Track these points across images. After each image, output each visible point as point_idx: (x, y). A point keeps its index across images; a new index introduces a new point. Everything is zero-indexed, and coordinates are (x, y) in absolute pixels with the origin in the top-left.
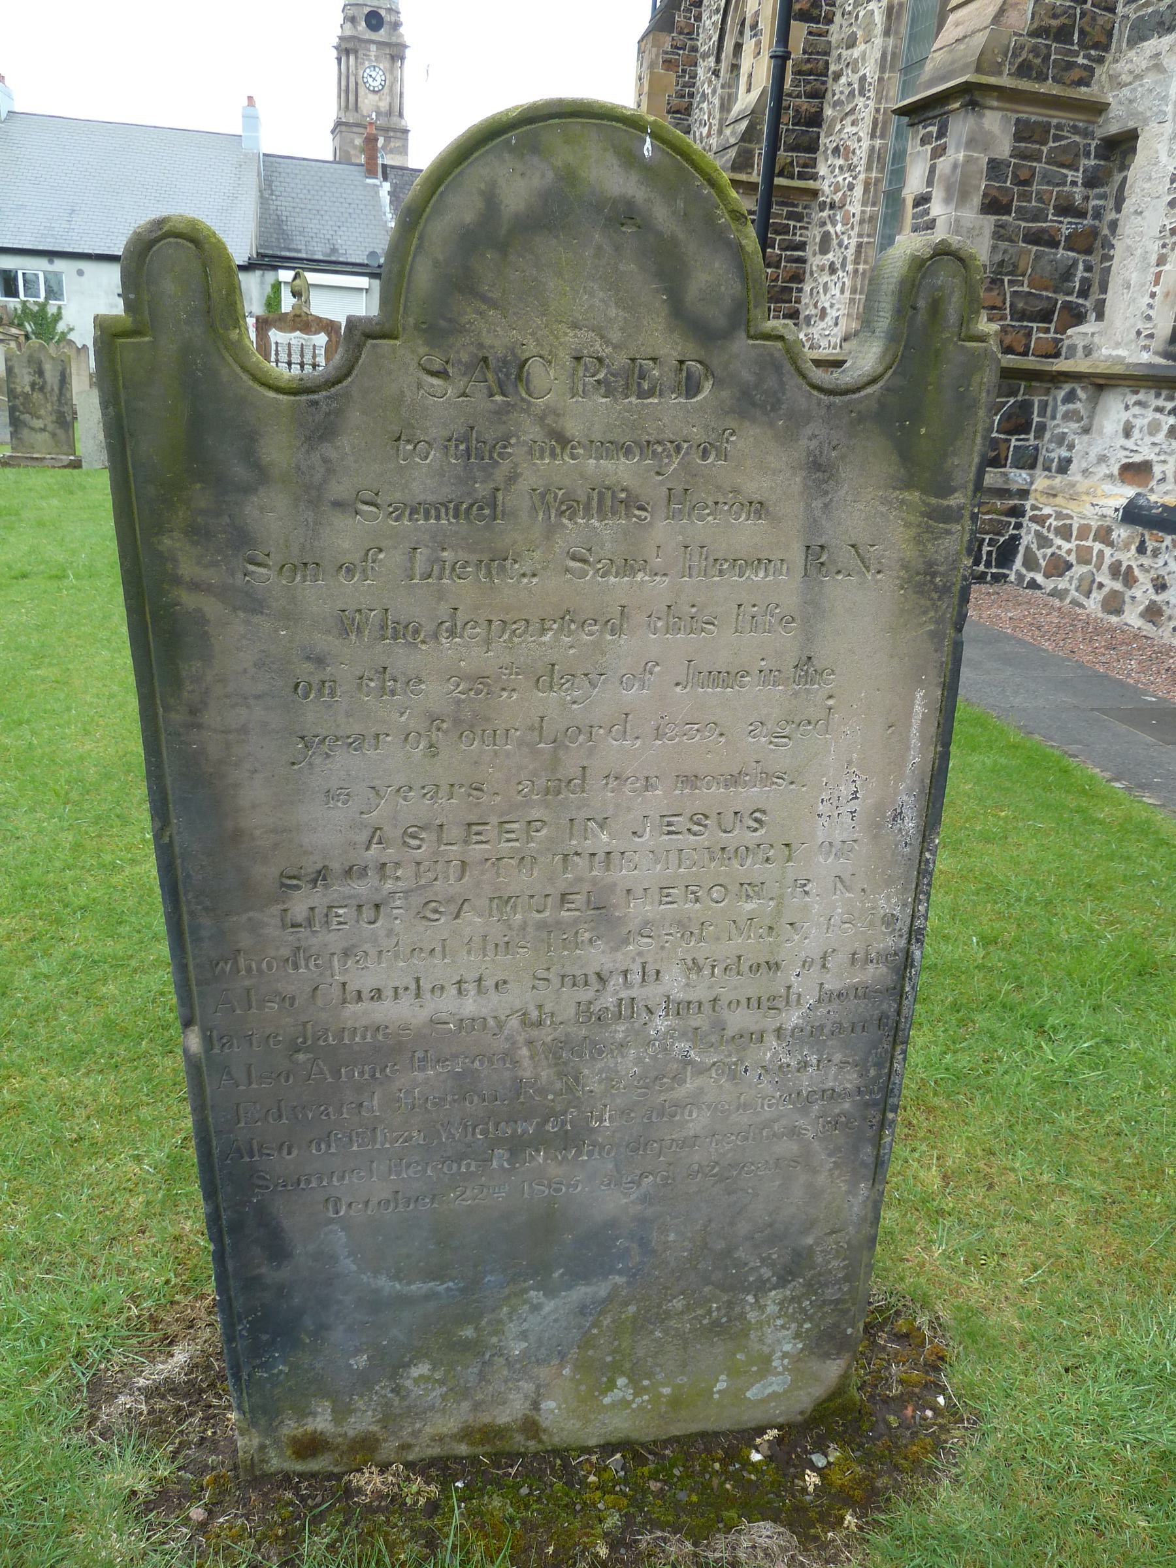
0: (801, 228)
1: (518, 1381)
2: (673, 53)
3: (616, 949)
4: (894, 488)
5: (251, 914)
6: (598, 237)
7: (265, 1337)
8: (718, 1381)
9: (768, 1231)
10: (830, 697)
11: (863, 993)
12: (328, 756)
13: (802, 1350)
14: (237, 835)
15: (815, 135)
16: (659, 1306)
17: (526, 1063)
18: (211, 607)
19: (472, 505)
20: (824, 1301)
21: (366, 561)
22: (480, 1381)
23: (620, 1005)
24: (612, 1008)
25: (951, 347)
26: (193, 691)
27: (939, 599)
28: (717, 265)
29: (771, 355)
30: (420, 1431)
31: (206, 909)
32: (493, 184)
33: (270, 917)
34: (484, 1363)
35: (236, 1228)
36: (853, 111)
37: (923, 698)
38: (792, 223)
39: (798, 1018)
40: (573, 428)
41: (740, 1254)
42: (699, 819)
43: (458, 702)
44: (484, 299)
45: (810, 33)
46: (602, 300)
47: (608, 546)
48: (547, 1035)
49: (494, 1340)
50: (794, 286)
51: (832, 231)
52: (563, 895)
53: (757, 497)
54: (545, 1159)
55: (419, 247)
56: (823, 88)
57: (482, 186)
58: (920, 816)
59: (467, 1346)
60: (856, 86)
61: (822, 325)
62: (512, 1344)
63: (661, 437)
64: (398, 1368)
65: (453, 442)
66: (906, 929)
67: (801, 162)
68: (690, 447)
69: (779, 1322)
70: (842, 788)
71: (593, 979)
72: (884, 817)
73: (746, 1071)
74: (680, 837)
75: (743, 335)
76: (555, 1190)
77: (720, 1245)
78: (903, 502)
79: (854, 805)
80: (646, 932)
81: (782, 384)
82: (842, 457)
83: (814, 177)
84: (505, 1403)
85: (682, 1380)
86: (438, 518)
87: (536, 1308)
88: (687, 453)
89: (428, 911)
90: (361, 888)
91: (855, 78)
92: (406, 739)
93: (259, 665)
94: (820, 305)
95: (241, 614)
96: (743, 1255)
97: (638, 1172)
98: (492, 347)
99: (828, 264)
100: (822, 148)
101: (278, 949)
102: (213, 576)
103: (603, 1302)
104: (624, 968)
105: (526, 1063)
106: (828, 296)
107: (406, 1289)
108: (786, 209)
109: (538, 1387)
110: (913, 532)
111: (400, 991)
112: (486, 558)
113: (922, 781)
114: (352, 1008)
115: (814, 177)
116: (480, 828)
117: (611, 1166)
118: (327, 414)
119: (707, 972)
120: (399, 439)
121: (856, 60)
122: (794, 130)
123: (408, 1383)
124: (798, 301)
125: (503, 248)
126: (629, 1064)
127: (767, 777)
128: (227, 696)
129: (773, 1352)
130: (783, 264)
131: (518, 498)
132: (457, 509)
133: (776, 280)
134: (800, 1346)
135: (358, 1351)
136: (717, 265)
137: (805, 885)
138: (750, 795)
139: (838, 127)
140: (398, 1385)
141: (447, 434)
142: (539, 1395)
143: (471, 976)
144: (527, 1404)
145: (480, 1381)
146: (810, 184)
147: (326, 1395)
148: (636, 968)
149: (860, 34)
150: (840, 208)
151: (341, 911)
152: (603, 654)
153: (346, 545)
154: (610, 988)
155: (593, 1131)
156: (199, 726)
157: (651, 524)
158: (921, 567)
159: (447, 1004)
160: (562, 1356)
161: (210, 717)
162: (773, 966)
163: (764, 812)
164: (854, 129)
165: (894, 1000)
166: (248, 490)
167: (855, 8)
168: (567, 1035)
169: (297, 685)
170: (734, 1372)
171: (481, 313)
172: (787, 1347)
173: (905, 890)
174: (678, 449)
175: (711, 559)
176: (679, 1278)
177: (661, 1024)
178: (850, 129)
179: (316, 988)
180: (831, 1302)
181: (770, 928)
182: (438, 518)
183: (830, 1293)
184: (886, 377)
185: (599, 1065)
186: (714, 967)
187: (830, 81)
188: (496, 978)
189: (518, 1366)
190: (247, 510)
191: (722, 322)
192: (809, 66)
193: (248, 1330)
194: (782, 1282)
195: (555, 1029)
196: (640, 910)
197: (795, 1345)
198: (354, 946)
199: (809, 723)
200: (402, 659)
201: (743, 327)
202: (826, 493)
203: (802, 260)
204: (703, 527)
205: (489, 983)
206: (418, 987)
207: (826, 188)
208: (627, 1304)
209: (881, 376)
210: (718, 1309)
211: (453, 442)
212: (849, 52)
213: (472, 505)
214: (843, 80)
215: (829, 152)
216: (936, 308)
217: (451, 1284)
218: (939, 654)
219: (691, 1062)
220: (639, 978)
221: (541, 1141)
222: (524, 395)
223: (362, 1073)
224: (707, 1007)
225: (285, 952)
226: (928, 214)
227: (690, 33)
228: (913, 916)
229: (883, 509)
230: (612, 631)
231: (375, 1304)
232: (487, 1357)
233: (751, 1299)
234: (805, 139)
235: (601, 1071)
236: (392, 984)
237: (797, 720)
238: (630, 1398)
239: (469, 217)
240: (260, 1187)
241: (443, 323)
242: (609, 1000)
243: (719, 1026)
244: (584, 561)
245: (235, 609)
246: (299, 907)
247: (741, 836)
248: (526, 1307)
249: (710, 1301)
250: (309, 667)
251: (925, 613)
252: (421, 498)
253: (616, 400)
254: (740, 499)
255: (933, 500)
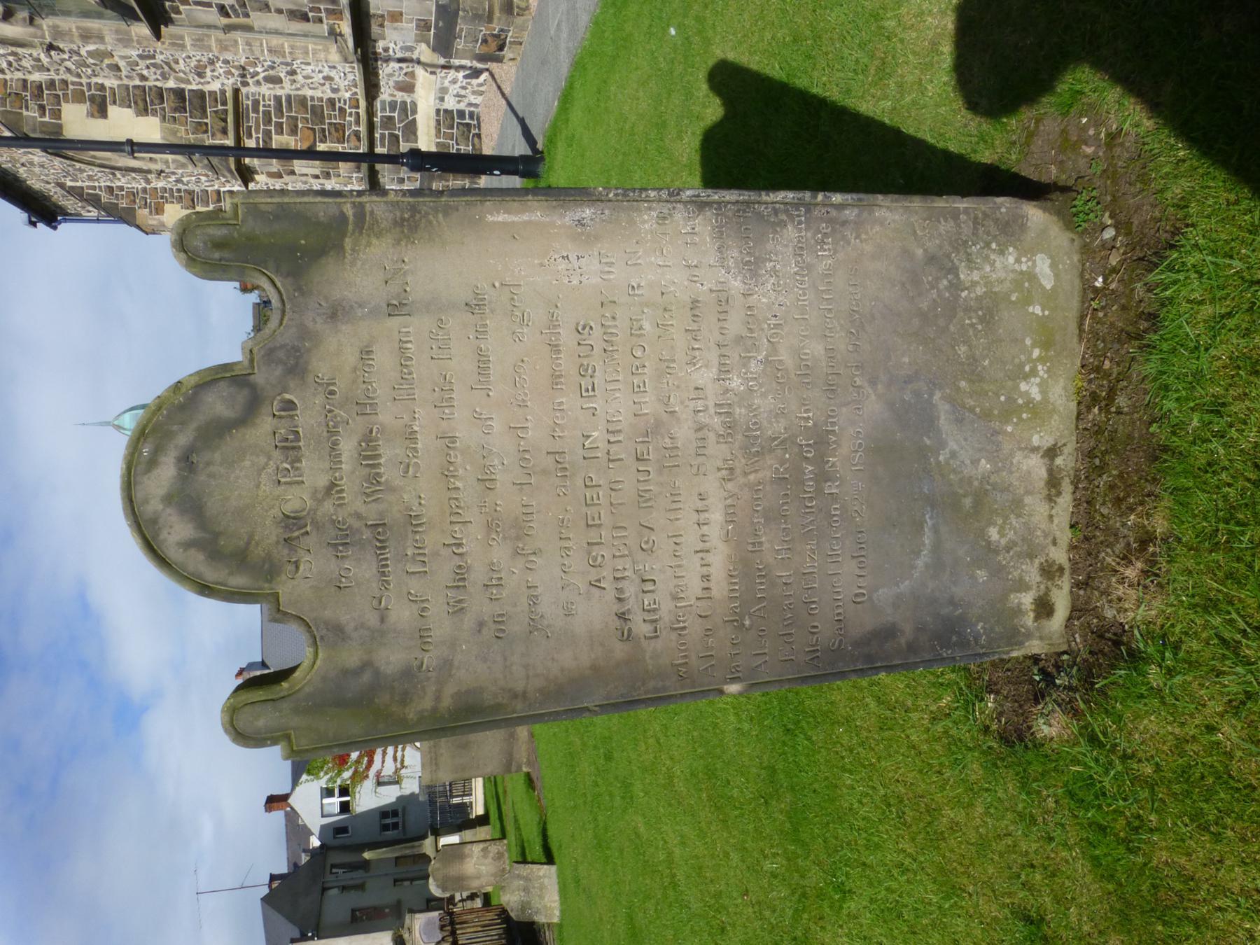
0: (264, 100)
1: (1012, 463)
2: (150, 206)
3: (678, 420)
4: (344, 258)
5: (647, 658)
6: (203, 478)
7: (954, 638)
8: (1033, 313)
9: (908, 286)
10: (494, 286)
11: (719, 234)
12: (542, 616)
13: (1015, 248)
14: (595, 668)
15: (191, 93)
16: (962, 364)
17: (760, 475)
18: (450, 690)
19: (377, 539)
20: (973, 234)
21: (416, 601)
22: (1009, 491)
23: (720, 413)
24: (722, 419)
25: (244, 230)
26: (503, 698)
27: (420, 213)
28: (210, 400)
29: (263, 356)
30: (1044, 531)
31: (643, 685)
32: (179, 544)
33: (649, 647)
34: (994, 489)
35: (869, 658)
36: (167, 63)
37: (492, 214)
38: (261, 109)
39: (736, 280)
40: (323, 481)
41: (924, 305)
42: (583, 371)
43: (504, 538)
44: (248, 543)
45: (114, 102)
46: (241, 471)
47: (398, 451)
48: (740, 463)
49: (976, 483)
50: (309, 103)
51: (262, 75)
52: (638, 459)
53: (358, 354)
54: (836, 456)
55: (221, 584)
56: (154, 89)
57: (181, 550)
58: (582, 205)
59: (978, 503)
60: (148, 62)
61: (337, 78)
62: (980, 470)
63: (324, 424)
64: (991, 549)
65: (339, 554)
66: (670, 206)
67: (213, 104)
68: (329, 404)
69: (988, 268)
70: (560, 268)
71: (700, 435)
72: (582, 233)
73: (776, 316)
74: (596, 382)
75: (252, 376)
76: (859, 447)
77: (916, 322)
78: (353, 250)
79: (573, 258)
80: (666, 400)
81: (282, 347)
82: (326, 299)
83: (223, 92)
84: (1029, 472)
85: (1028, 342)
86: (386, 559)
87: (953, 455)
88: (333, 406)
89: (648, 550)
90: (631, 589)
91: (142, 64)
92: (530, 569)
93: (485, 660)
94: (322, 81)
95: (454, 671)
96: (926, 304)
97: (851, 389)
98: (277, 536)
99: (288, 77)
100: (200, 87)
101: (671, 640)
102: (431, 689)
103: (954, 406)
104: (693, 414)
105: (760, 475)
106: (313, 75)
107: (928, 547)
108: (251, 115)
109: (1020, 449)
110: (374, 241)
111: (704, 562)
112: (410, 528)
113: (554, 207)
114: (715, 593)
115: (223, 92)
116: (589, 518)
117: (844, 410)
118: (328, 629)
119: (697, 353)
120: (339, 587)
121: (128, 63)
122: (190, 112)
123: (1003, 541)
124: (321, 100)
125: (217, 535)
126: (765, 403)
127: (553, 325)
128: (505, 677)
129: (1014, 271)
130: (293, 114)
131: (371, 512)
132: (380, 548)
133: (306, 119)
134: (1011, 249)
135: (973, 577)
136: (210, 400)
137: (633, 287)
138: (567, 337)
139: (182, 75)
140: (1004, 549)
141: (334, 559)
142: (1026, 448)
143: (695, 517)
144: (1032, 456)
145: (1009, 491)
146: (229, 95)
147: (1005, 597)
148: (692, 404)
149: (107, 61)
150: (244, 69)
151: (646, 603)
152: (469, 447)
153: (407, 613)
154: (707, 421)
155: (815, 425)
156: (525, 692)
157: (381, 425)
158: (398, 229)
159: (715, 532)
160: (997, 433)
161: (520, 686)
162: (695, 303)
163: (578, 324)
164: (181, 62)
165: (725, 206)
166: (377, 673)
167: (88, 66)
168: (741, 448)
169: (497, 637)
170: (1028, 301)
171: (257, 544)
172: (1011, 259)
173: (638, 210)
174: (330, 411)
175: (402, 381)
176: (941, 351)
177: (736, 383)
178: (182, 65)
179: (700, 616)
180: (975, 228)
181: (665, 310)
182: (386, 559)
183: (967, 230)
184: (269, 274)
185: (765, 423)
186: (693, 349)
187: (148, 84)
188: (697, 500)
189: (1000, 464)
190: (389, 672)
191: (246, 392)
192: (140, 102)
193: (948, 649)
194: (954, 270)
195: (736, 457)
196: (650, 405)
197: (1010, 254)
198: (671, 594)
199: (513, 299)
200: (478, 575)
201: (247, 377)
202: (351, 307)
203: (289, 97)
204: (381, 391)
205: (700, 505)
206: (701, 551)
207: (232, 81)
208: (958, 389)
209: (269, 278)
210: (970, 318)
211: (339, 554)
212: (122, 69)
213: (377, 539)
214: (145, 72)
215: (202, 81)
216: (219, 245)
217: (927, 516)
218: (460, 208)
219: (766, 358)
220: (700, 402)
221: (820, 460)
222: (305, 513)
223: (762, 583)
224: (724, 351)
225: (674, 636)
226: (233, 6)
227: (133, 194)
228: (660, 201)
229: (359, 263)
230: (453, 443)
231: (937, 566)
232: (989, 487)
233: (964, 294)
234: (196, 102)
235: (770, 422)
236: (699, 568)
237: (510, 308)
238: (1038, 380)
239: (200, 557)
240: (840, 646)
241: (266, 566)
242: (717, 420)
243: (739, 339)
244: (408, 465)
245: (450, 676)
246: (641, 628)
247: (596, 338)
248: (952, 462)
249: (963, 326)
250: (485, 631)
251: (430, 222)
252: (375, 571)
253: (302, 456)
254: (360, 366)
255: (350, 227)
